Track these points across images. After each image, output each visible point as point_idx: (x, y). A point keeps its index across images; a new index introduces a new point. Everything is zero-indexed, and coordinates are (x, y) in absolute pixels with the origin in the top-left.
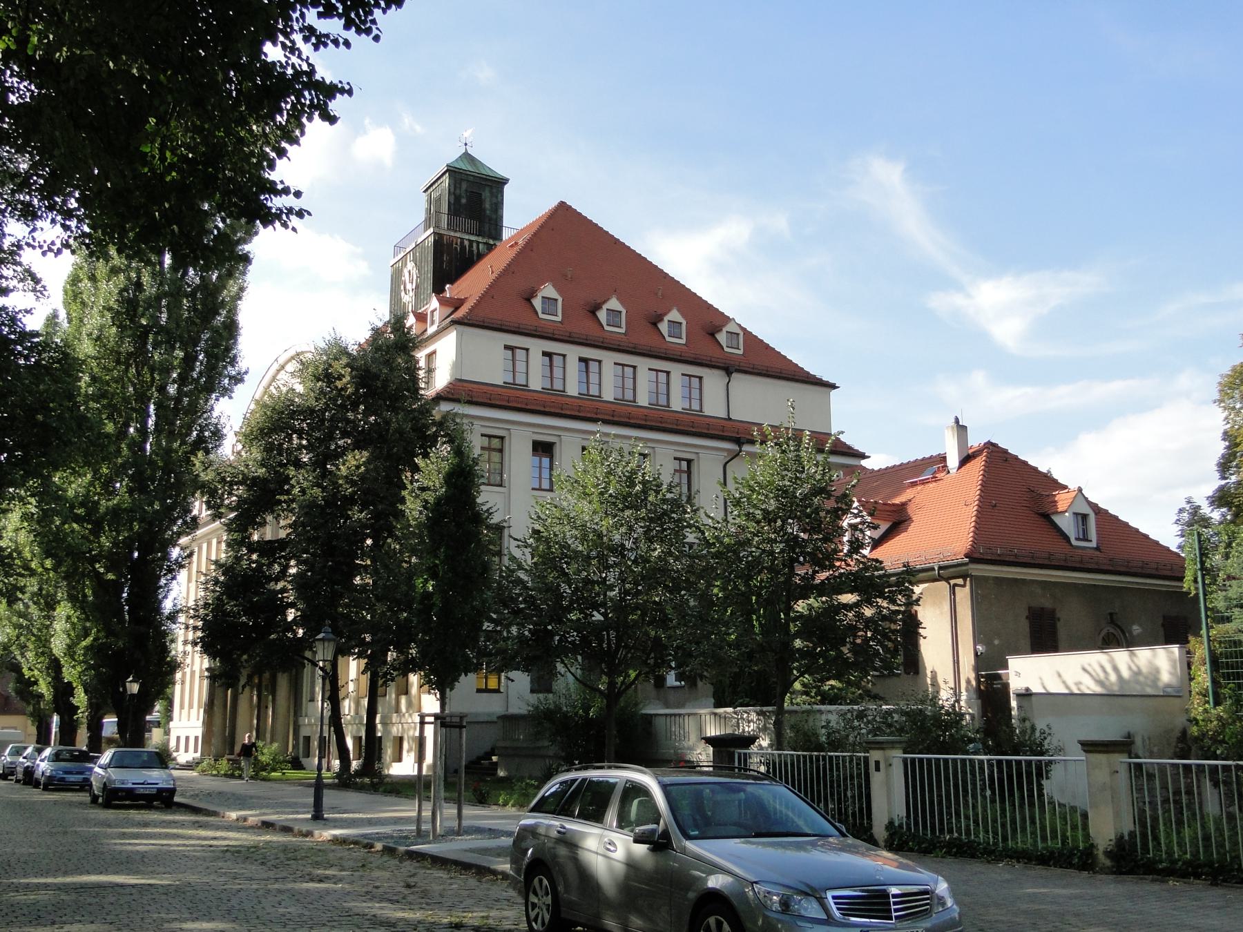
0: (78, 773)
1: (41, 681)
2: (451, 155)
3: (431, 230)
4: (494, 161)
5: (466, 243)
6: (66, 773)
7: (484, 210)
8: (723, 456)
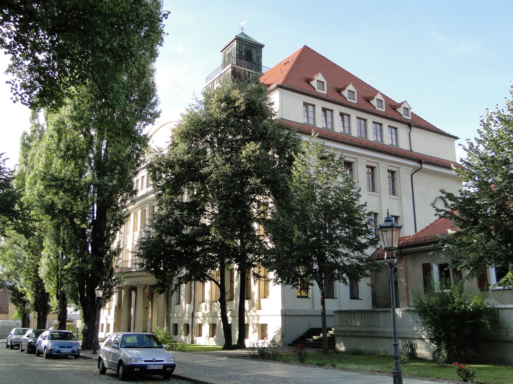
0: (69, 347)
1: (28, 294)
2: (237, 32)
3: (230, 65)
4: (256, 37)
5: (247, 73)
6: (61, 347)
7: (253, 59)
8: (410, 170)
